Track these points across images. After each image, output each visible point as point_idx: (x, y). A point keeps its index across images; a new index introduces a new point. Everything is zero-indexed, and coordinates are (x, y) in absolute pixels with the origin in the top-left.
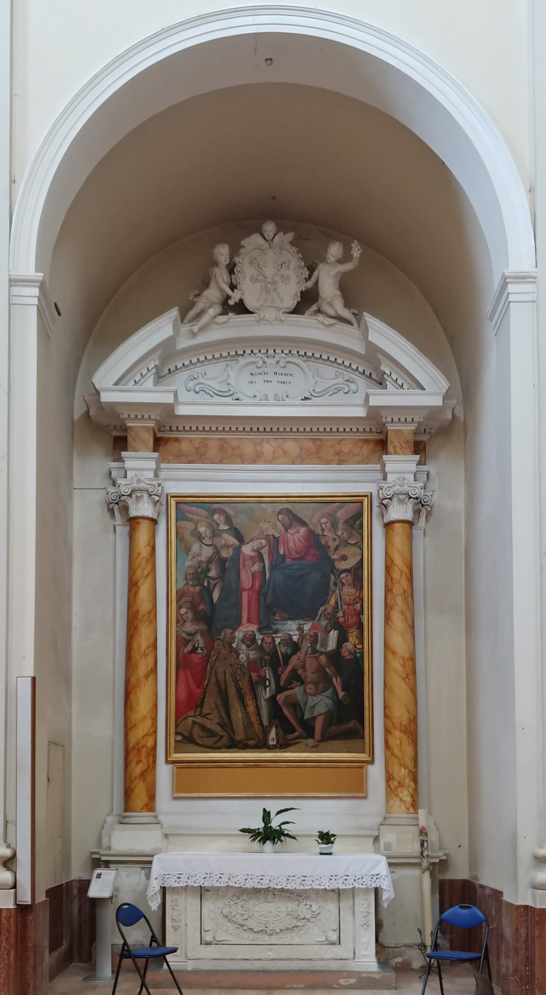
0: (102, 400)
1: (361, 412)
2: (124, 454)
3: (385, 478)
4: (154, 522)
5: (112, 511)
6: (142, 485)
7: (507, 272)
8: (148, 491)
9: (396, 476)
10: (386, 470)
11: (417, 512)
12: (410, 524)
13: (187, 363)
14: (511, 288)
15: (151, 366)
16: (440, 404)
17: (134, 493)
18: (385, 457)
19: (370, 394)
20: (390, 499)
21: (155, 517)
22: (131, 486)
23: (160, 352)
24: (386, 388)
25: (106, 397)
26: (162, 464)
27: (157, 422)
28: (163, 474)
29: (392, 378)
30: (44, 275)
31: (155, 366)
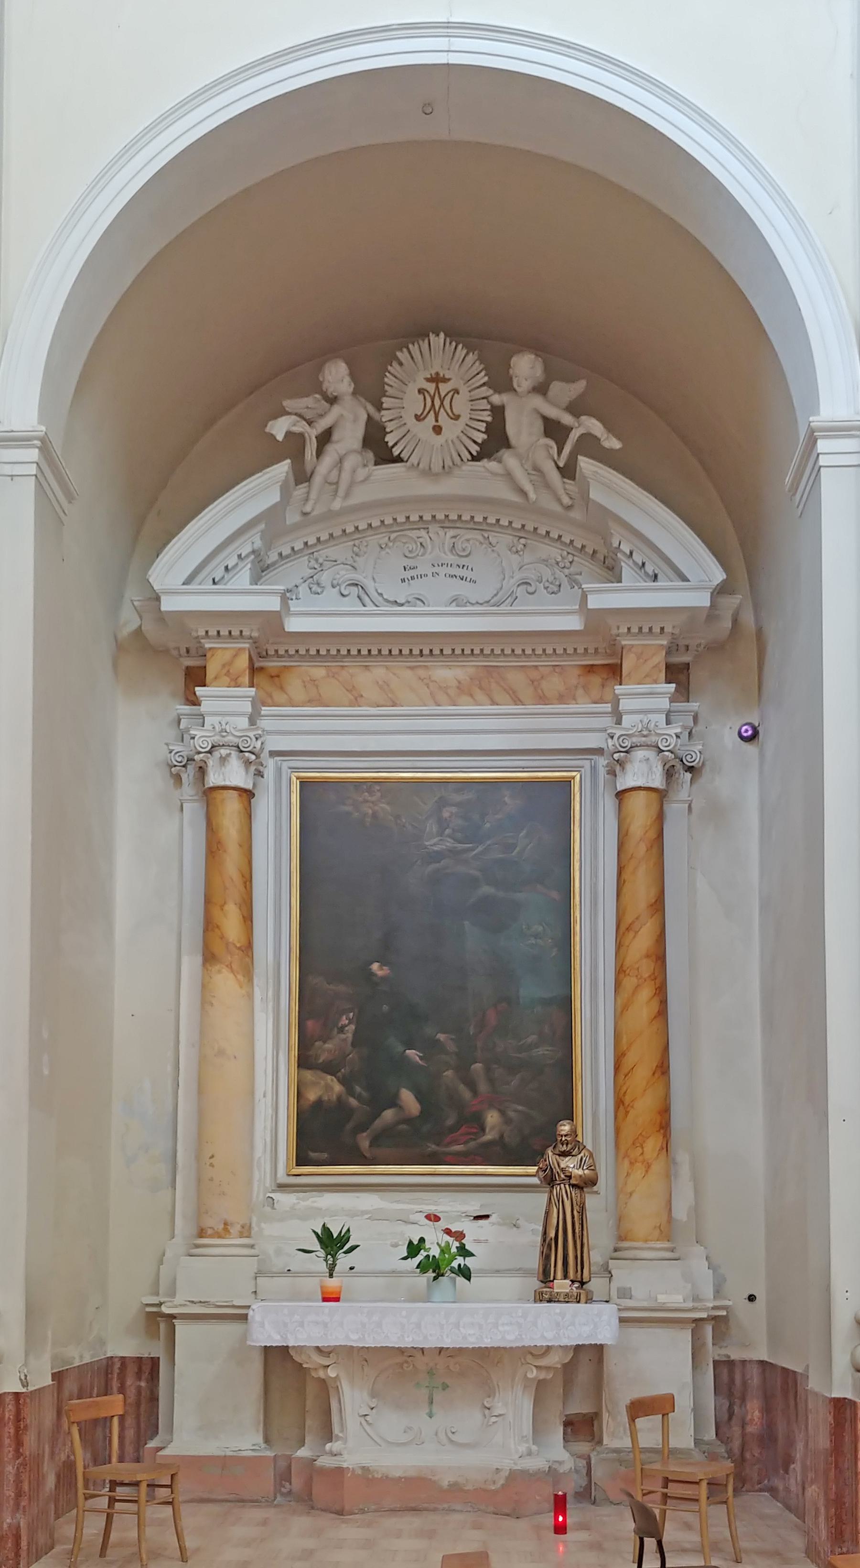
0: (163, 608)
1: (574, 623)
2: (199, 690)
3: (619, 722)
4: (247, 795)
5: (178, 779)
6: (230, 738)
7: (816, 421)
8: (238, 747)
9: (637, 718)
10: (620, 708)
11: (669, 773)
12: (661, 795)
13: (376, 523)
14: (822, 445)
15: (245, 550)
16: (707, 604)
17: (217, 750)
18: (619, 689)
19: (588, 591)
20: (626, 752)
21: (250, 786)
22: (212, 738)
23: (262, 526)
24: (620, 581)
25: (168, 604)
26: (263, 708)
27: (255, 641)
28: (265, 724)
29: (646, 573)
30: (47, 429)
31: (253, 552)
